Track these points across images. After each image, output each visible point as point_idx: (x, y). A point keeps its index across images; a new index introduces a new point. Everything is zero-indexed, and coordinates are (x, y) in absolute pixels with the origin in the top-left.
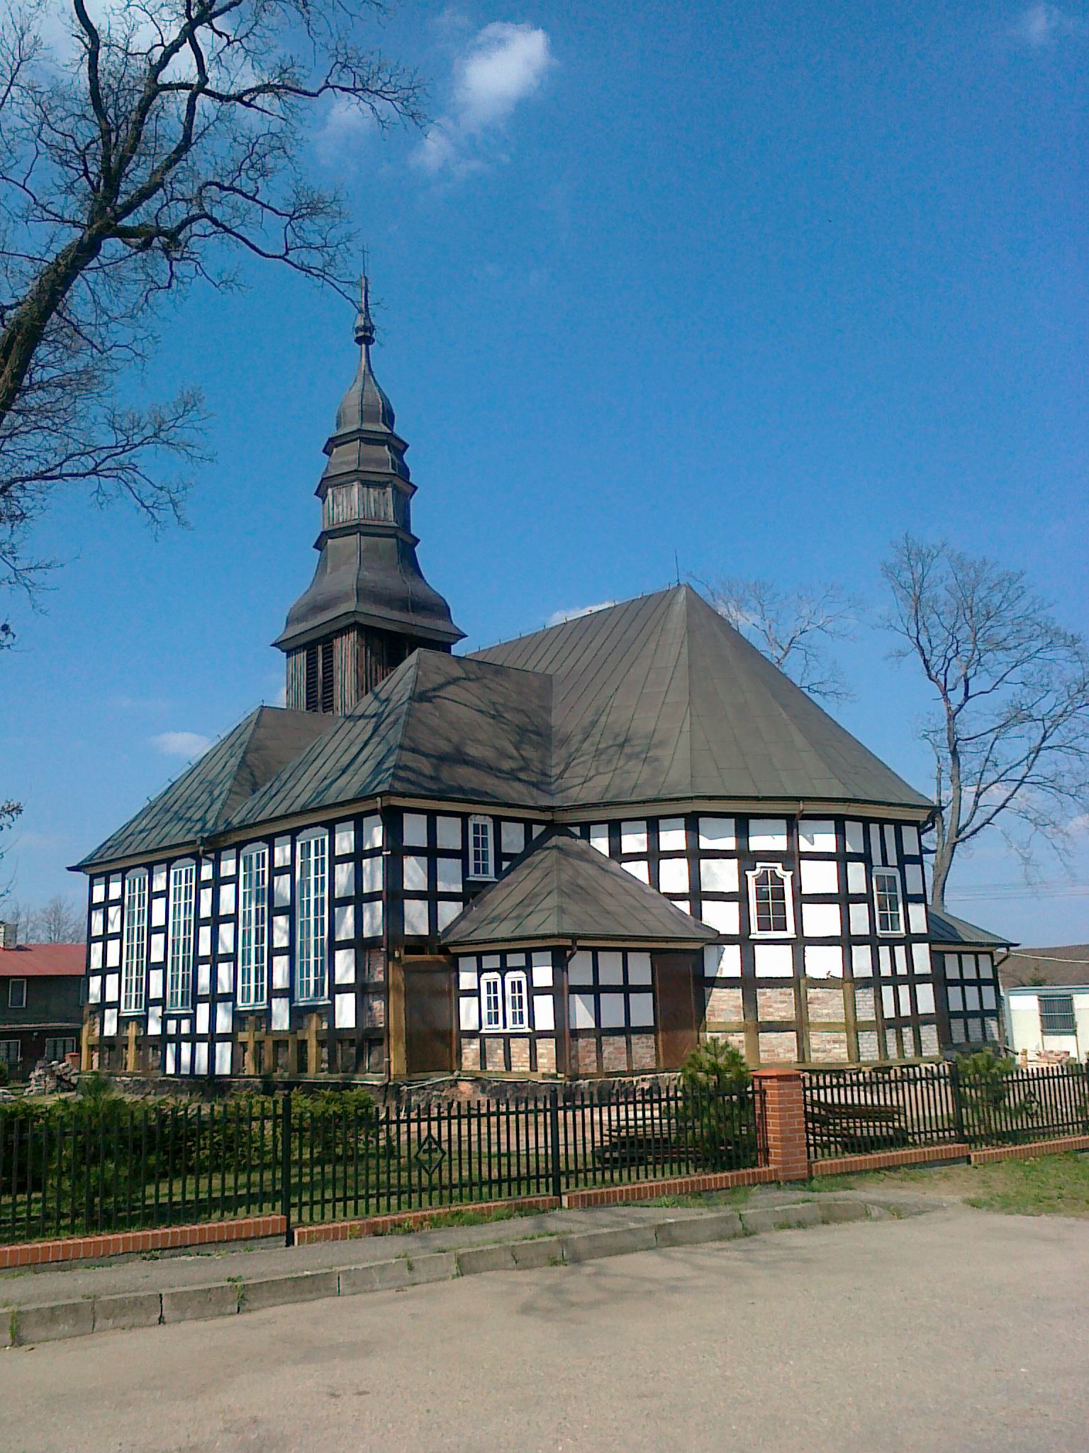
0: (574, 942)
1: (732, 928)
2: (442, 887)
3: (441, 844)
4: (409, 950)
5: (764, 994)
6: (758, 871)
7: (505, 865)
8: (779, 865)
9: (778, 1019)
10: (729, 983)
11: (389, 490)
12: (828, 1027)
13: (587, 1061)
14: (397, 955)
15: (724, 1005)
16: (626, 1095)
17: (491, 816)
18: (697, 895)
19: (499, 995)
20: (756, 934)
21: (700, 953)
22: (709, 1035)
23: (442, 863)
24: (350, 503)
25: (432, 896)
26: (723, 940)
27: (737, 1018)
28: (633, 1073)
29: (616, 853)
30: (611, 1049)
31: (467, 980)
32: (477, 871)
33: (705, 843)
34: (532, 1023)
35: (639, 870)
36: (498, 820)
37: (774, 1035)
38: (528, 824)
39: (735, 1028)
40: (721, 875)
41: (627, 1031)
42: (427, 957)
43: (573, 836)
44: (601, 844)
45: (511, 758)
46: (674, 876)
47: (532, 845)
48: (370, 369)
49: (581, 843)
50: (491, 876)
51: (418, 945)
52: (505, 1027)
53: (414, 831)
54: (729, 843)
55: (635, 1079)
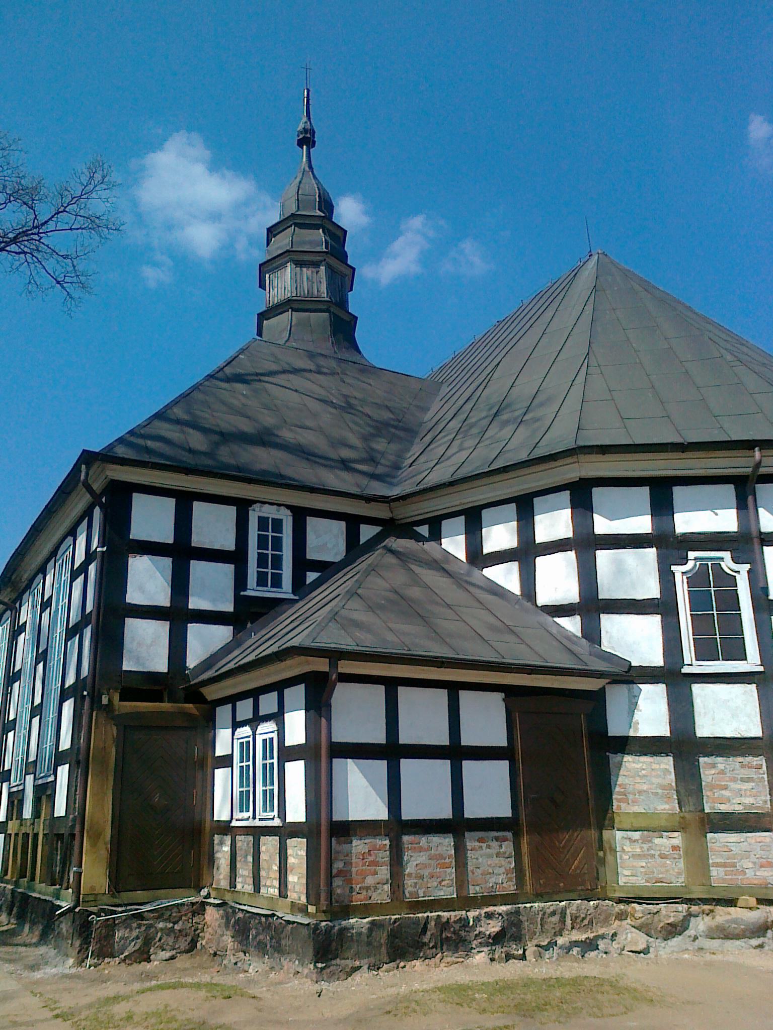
0: (333, 665)
1: (654, 657)
2: (195, 603)
3: (198, 539)
4: (126, 696)
5: (714, 766)
6: (690, 564)
7: (311, 576)
8: (727, 555)
9: (739, 809)
10: (651, 746)
11: (323, 268)
12: (652, 827)
13: (370, 881)
14: (105, 700)
15: (642, 783)
17: (288, 507)
18: (592, 606)
19: (251, 763)
21: (598, 699)
22: (619, 835)
23: (198, 568)
24: (284, 283)
25: (178, 616)
26: (632, 676)
27: (668, 806)
28: (466, 902)
29: (478, 558)
30: (422, 858)
31: (224, 741)
32: (262, 580)
33: (602, 525)
34: (282, 814)
35: (506, 576)
36: (300, 515)
37: (733, 837)
38: (353, 523)
39: (663, 823)
40: (632, 573)
41: (457, 826)
42: (165, 706)
43: (419, 538)
44: (455, 545)
45: (351, 447)
46: (557, 579)
47: (355, 548)
48: (311, 167)
49: (430, 546)
50: (286, 589)
51: (148, 686)
53: (151, 519)
54: (642, 524)
55: (472, 914)
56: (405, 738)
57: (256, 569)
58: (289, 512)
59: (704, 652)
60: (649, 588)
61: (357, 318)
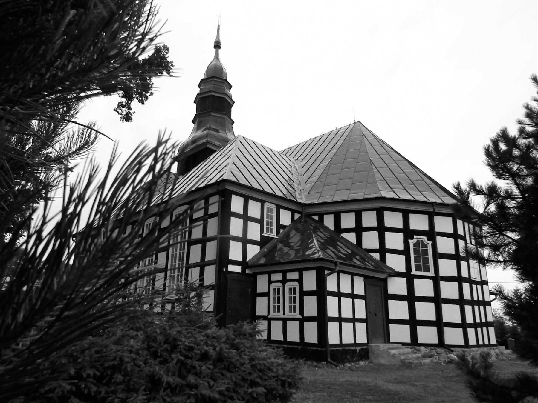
1: (403, 269)
16: (61, 53)
17: (275, 204)
20: (414, 272)
21: (385, 281)
32: (268, 231)
38: (293, 212)
40: (394, 241)
52: (284, 314)
56: (456, 284)
57: (429, 257)
58: (275, 206)
59: (418, 268)
60: (401, 246)
61: (231, 86)
